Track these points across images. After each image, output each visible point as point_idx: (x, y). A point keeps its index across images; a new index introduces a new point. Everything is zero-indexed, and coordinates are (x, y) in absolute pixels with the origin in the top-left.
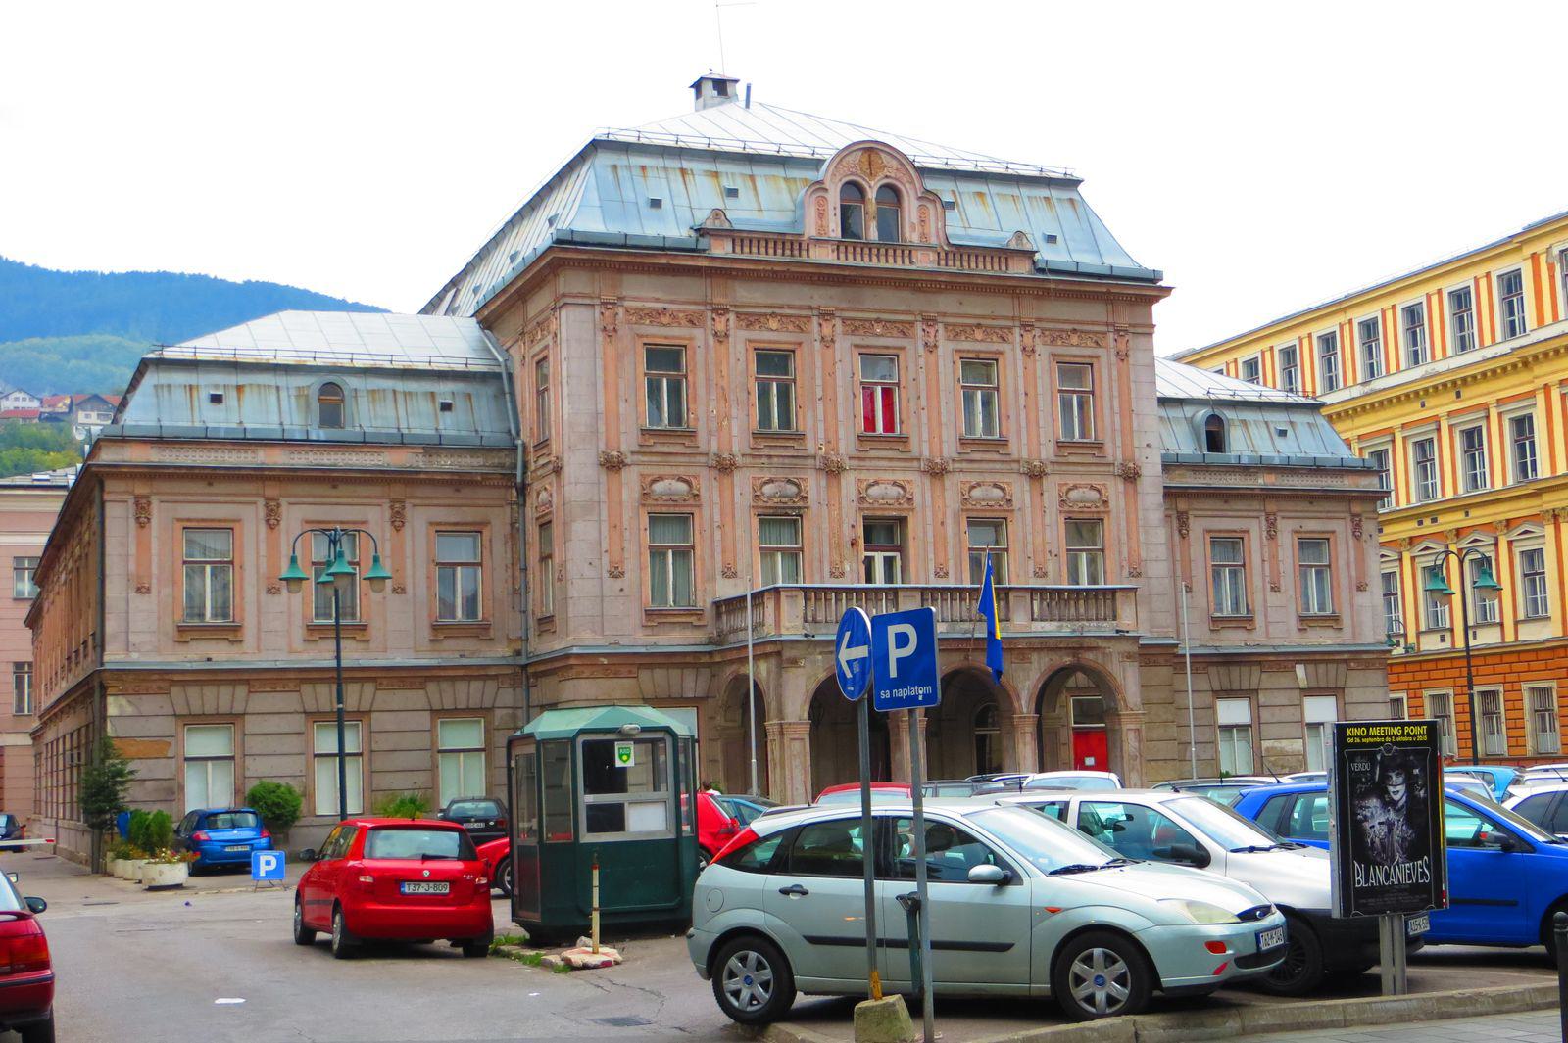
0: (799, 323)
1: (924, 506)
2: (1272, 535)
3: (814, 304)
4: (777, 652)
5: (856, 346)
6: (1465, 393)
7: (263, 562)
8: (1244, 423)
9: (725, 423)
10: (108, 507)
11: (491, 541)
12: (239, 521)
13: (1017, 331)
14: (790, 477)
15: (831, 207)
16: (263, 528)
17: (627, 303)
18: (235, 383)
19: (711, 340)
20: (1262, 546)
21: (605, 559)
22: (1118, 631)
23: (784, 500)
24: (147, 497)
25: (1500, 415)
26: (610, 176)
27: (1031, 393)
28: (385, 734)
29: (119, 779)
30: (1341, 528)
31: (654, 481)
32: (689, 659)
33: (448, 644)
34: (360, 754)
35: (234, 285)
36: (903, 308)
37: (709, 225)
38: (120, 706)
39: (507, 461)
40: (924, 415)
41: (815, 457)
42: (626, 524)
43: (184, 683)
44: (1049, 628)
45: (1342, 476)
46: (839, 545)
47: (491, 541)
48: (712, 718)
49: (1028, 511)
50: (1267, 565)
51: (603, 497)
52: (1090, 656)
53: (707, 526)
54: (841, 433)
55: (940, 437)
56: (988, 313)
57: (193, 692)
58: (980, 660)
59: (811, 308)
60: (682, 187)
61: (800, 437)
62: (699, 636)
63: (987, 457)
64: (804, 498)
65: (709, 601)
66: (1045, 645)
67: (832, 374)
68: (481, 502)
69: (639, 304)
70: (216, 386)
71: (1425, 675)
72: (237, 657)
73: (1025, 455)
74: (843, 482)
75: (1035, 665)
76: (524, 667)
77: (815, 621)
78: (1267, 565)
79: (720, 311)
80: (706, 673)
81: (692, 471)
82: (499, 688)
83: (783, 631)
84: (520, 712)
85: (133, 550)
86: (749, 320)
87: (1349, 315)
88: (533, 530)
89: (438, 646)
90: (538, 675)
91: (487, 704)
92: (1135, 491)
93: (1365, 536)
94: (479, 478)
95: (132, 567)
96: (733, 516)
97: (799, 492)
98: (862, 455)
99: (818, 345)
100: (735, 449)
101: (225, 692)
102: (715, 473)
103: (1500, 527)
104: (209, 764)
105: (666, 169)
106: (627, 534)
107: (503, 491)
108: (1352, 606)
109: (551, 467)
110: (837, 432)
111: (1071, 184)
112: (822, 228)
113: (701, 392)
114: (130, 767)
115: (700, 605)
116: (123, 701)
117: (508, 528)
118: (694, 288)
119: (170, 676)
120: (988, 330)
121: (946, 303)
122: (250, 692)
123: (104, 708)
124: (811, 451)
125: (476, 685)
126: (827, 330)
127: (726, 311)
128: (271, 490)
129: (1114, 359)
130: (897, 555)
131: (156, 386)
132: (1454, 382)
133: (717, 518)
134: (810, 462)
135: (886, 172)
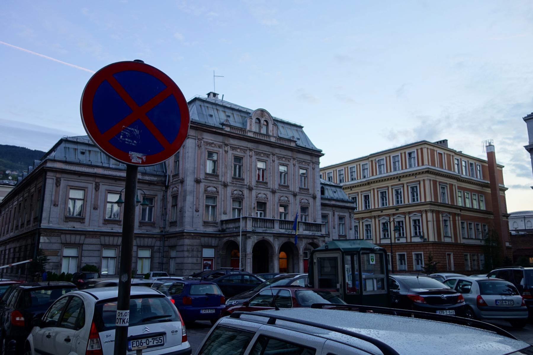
0: (244, 150)
1: (270, 200)
2: (334, 215)
3: (248, 147)
4: (246, 234)
5: (257, 158)
6: (353, 189)
7: (93, 200)
8: (327, 189)
9: (226, 174)
11: (157, 200)
12: (87, 188)
13: (292, 160)
14: (241, 190)
15: (253, 124)
16: (94, 190)
17: (204, 140)
18: (88, 149)
19: (224, 152)
20: (332, 218)
21: (195, 206)
22: (322, 235)
23: (239, 195)
24: (60, 178)
25: (361, 195)
26: (200, 108)
29: (43, 262)
30: (347, 215)
31: (208, 187)
32: (214, 235)
33: (144, 228)
34: (116, 257)
35: (32, 151)
36: (267, 150)
37: (225, 123)
38: (45, 240)
39: (163, 179)
40: (271, 177)
42: (200, 198)
43: (65, 234)
44: (307, 233)
45: (348, 203)
46: (251, 209)
47: (157, 200)
48: (219, 252)
49: (293, 204)
50: (333, 222)
51: (195, 190)
52: (315, 240)
53: (220, 201)
54: (253, 180)
56: (286, 154)
57: (68, 236)
58: (293, 240)
59: (247, 148)
60: (217, 113)
61: (243, 180)
62: (216, 229)
64: (244, 195)
65: (219, 220)
66: (306, 237)
67: (251, 165)
68: (155, 190)
69: (207, 140)
70: (83, 150)
71: (413, 248)
72: (83, 227)
73: (293, 190)
74: (253, 192)
75: (304, 242)
76: (164, 235)
77: (255, 227)
78: (333, 222)
79: (226, 145)
80: (218, 239)
81: (217, 185)
82: (156, 241)
83: (247, 229)
84: (161, 248)
85: (54, 193)
86: (233, 148)
87: (325, 171)
88: (170, 199)
90: (168, 238)
91: (153, 245)
92: (315, 202)
93: (352, 217)
94: (156, 183)
96: (227, 198)
98: (257, 186)
99: (248, 157)
100: (228, 181)
101: (78, 237)
102: (223, 187)
103: (391, 215)
104: (70, 258)
105: (213, 108)
106: (200, 200)
107: (161, 187)
108: (349, 233)
109: (179, 181)
111: (301, 127)
112: (251, 128)
113: (221, 165)
114: (48, 258)
115: (217, 221)
116: (45, 238)
118: (220, 138)
119: (61, 231)
120: (286, 158)
121: (277, 151)
122: (85, 238)
123: (39, 239)
124: (246, 184)
126: (251, 153)
128: (97, 180)
129: (312, 169)
130: (263, 212)
131: (65, 147)
132: (351, 187)
133: (223, 198)
134: (245, 186)
135: (265, 117)
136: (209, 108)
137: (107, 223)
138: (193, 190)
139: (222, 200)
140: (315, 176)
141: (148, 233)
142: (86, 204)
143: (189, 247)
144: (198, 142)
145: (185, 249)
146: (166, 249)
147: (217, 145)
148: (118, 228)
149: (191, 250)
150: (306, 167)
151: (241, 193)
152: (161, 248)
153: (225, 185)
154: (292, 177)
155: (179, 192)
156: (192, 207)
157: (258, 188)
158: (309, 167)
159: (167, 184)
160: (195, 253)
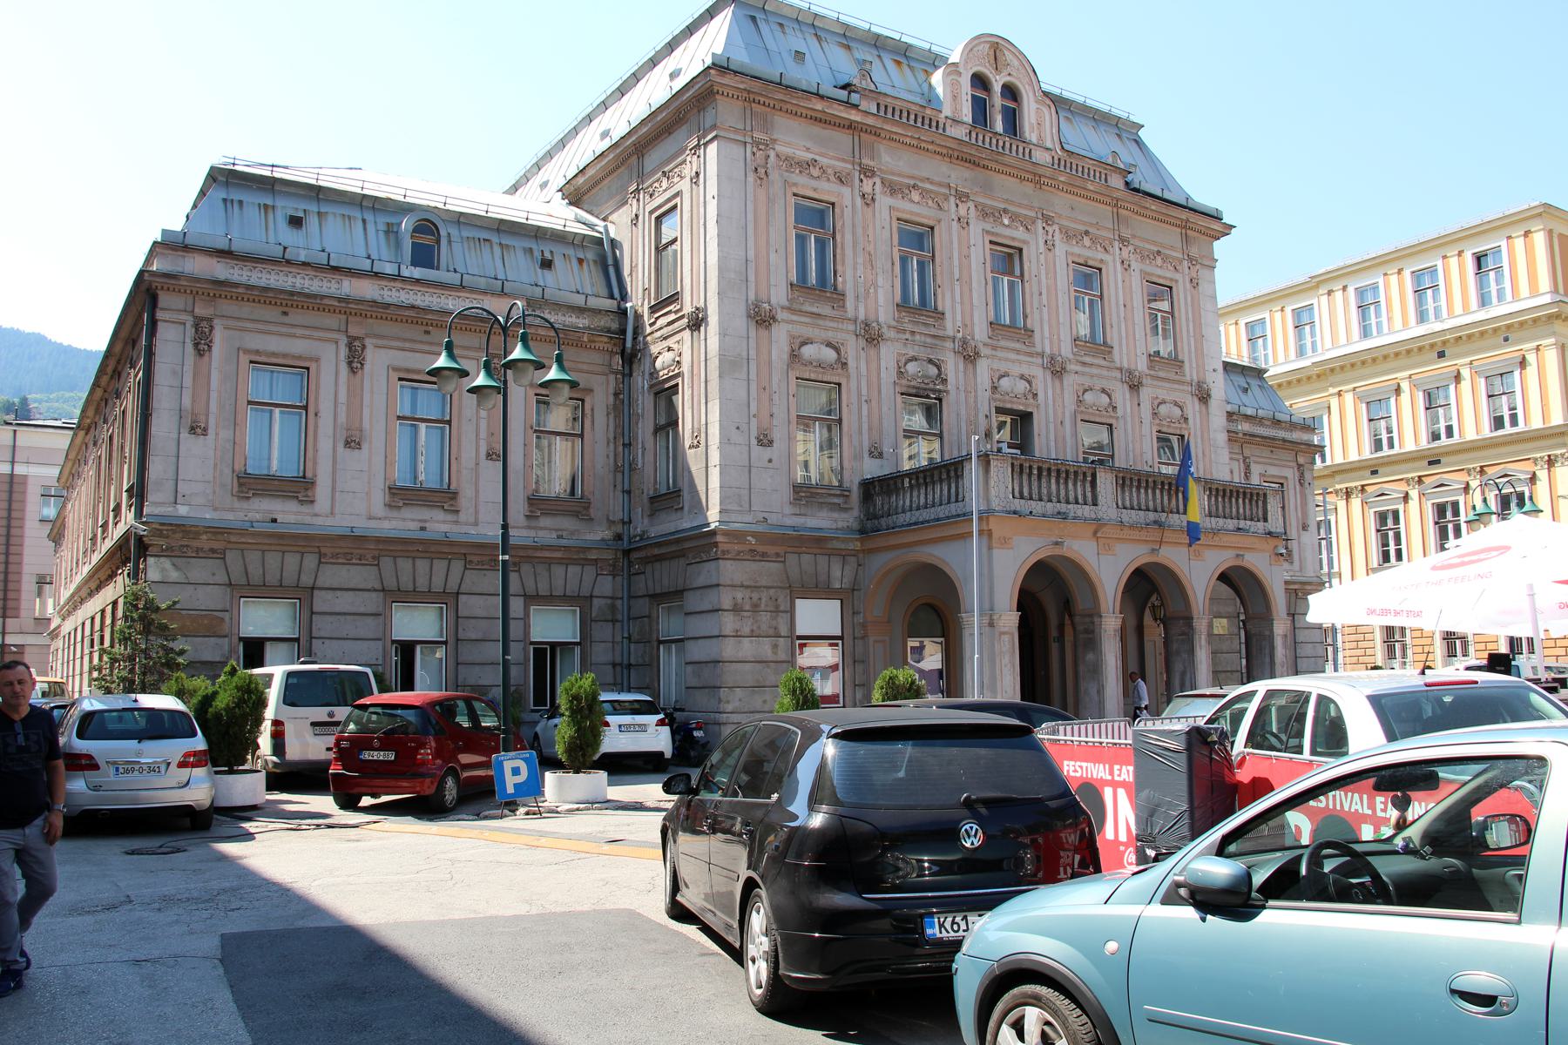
5: (988, 232)
7: (342, 410)
9: (872, 291)
10: (161, 327)
11: (592, 410)
19: (859, 201)
21: (754, 422)
24: (210, 320)
27: (1128, 306)
28: (473, 621)
31: (804, 344)
33: (545, 522)
38: (163, 570)
40: (1045, 310)
41: (954, 339)
42: (775, 387)
47: (592, 410)
51: (753, 353)
53: (854, 399)
55: (1059, 335)
63: (1096, 361)
64: (944, 381)
65: (856, 481)
67: (968, 256)
72: (308, 520)
76: (627, 553)
79: (867, 172)
84: (619, 603)
85: (188, 381)
89: (534, 523)
90: (648, 561)
91: (585, 592)
93: (1307, 484)
95: (187, 401)
97: (939, 375)
106: (776, 397)
110: (972, 316)
116: (166, 563)
117: (611, 399)
122: (320, 562)
124: (950, 332)
125: (574, 570)
126: (962, 211)
127: (873, 174)
131: (225, 200)
133: (864, 392)
134: (949, 344)
136: (787, 30)
137: (401, 504)
138: (744, 354)
139: (864, 398)
140: (1203, 313)
141: (563, 542)
142: (316, 426)
143: (739, 595)
144: (754, 154)
145: (727, 603)
146: (642, 606)
147: (830, 171)
148: (444, 522)
149: (747, 607)
150: (1169, 275)
151: (933, 371)
152: (619, 603)
153: (871, 336)
154: (1122, 315)
155: (685, 368)
156: (744, 427)
157: (1000, 354)
158: (1177, 276)
159: (629, 344)
160: (765, 618)
